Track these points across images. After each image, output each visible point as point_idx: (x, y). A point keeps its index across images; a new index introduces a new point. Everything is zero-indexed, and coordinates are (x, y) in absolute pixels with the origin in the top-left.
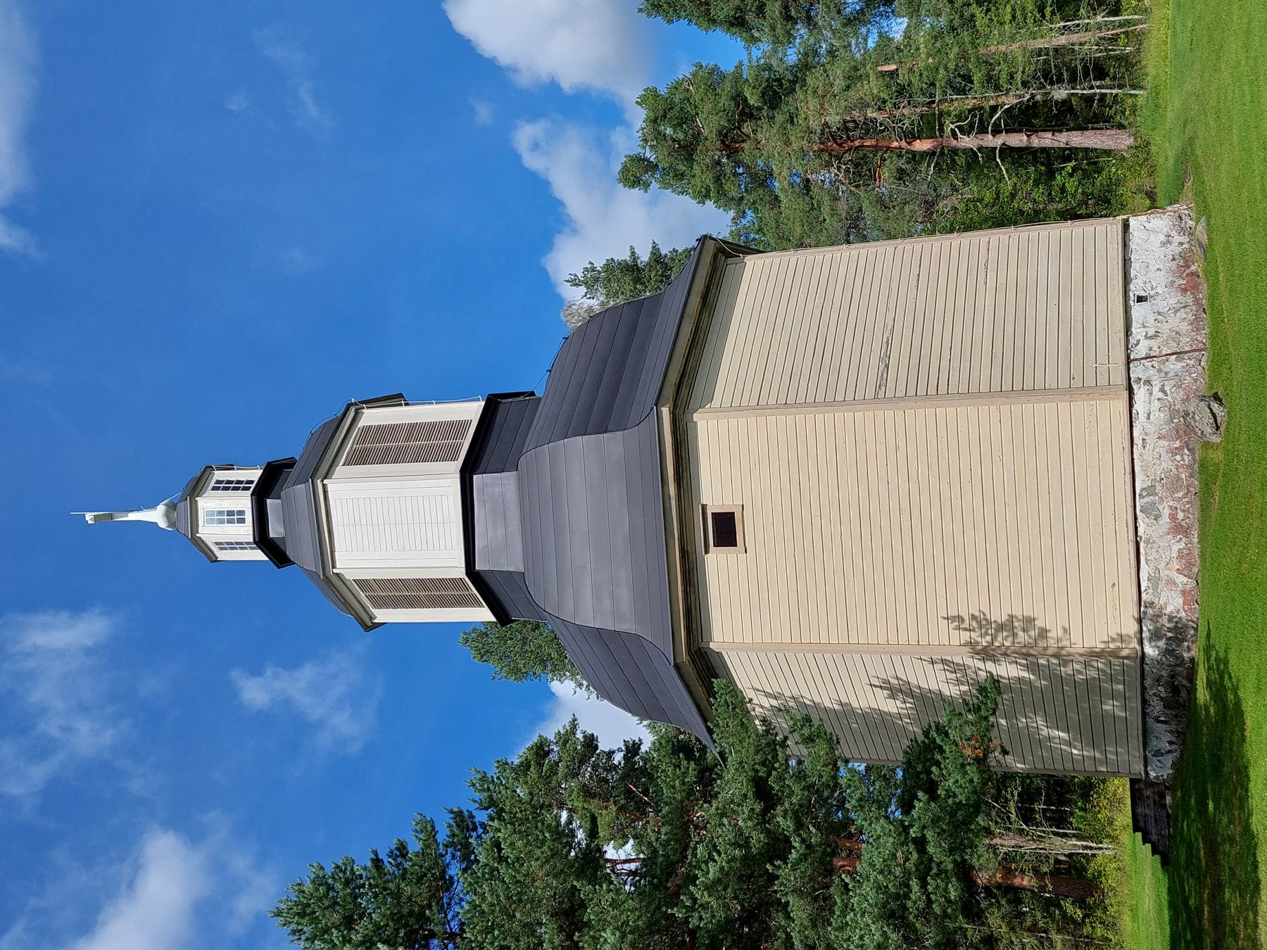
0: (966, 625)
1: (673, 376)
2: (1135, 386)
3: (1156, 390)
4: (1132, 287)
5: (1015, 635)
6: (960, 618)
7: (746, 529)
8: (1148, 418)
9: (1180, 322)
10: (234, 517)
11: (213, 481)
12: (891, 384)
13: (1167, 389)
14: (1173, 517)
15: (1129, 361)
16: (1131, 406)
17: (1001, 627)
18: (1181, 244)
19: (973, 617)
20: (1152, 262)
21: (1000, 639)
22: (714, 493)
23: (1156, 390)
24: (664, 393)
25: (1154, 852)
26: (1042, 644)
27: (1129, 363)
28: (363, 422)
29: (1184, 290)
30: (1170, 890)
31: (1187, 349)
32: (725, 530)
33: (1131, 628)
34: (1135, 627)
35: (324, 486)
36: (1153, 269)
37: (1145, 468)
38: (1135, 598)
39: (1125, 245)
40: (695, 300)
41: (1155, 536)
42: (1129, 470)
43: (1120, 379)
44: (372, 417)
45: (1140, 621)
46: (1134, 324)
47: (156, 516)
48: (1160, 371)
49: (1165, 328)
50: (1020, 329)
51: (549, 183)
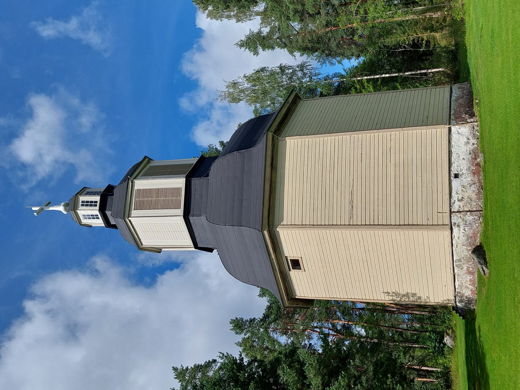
0: (391, 294)
2: (453, 227)
3: (462, 229)
4: (452, 169)
5: (409, 298)
6: (388, 293)
7: (304, 263)
8: (459, 238)
9: (471, 192)
11: (80, 202)
12: (355, 217)
13: (466, 229)
14: (468, 269)
15: (451, 212)
16: (452, 233)
17: (404, 296)
18: (473, 144)
19: (393, 292)
20: (461, 154)
21: (404, 299)
22: (290, 251)
23: (462, 229)
24: (264, 223)
25: (460, 316)
26: (419, 301)
27: (451, 214)
28: (136, 187)
29: (474, 174)
30: (466, 326)
31: (475, 209)
33: (452, 298)
34: (454, 298)
35: (130, 221)
36: (461, 158)
37: (457, 254)
38: (454, 290)
39: (449, 142)
40: (268, 169)
41: (461, 274)
42: (454, 156)
43: (447, 222)
44: (141, 184)
45: (455, 297)
46: (453, 191)
47: (61, 208)
48: (463, 220)
49: (466, 195)
50: (406, 190)
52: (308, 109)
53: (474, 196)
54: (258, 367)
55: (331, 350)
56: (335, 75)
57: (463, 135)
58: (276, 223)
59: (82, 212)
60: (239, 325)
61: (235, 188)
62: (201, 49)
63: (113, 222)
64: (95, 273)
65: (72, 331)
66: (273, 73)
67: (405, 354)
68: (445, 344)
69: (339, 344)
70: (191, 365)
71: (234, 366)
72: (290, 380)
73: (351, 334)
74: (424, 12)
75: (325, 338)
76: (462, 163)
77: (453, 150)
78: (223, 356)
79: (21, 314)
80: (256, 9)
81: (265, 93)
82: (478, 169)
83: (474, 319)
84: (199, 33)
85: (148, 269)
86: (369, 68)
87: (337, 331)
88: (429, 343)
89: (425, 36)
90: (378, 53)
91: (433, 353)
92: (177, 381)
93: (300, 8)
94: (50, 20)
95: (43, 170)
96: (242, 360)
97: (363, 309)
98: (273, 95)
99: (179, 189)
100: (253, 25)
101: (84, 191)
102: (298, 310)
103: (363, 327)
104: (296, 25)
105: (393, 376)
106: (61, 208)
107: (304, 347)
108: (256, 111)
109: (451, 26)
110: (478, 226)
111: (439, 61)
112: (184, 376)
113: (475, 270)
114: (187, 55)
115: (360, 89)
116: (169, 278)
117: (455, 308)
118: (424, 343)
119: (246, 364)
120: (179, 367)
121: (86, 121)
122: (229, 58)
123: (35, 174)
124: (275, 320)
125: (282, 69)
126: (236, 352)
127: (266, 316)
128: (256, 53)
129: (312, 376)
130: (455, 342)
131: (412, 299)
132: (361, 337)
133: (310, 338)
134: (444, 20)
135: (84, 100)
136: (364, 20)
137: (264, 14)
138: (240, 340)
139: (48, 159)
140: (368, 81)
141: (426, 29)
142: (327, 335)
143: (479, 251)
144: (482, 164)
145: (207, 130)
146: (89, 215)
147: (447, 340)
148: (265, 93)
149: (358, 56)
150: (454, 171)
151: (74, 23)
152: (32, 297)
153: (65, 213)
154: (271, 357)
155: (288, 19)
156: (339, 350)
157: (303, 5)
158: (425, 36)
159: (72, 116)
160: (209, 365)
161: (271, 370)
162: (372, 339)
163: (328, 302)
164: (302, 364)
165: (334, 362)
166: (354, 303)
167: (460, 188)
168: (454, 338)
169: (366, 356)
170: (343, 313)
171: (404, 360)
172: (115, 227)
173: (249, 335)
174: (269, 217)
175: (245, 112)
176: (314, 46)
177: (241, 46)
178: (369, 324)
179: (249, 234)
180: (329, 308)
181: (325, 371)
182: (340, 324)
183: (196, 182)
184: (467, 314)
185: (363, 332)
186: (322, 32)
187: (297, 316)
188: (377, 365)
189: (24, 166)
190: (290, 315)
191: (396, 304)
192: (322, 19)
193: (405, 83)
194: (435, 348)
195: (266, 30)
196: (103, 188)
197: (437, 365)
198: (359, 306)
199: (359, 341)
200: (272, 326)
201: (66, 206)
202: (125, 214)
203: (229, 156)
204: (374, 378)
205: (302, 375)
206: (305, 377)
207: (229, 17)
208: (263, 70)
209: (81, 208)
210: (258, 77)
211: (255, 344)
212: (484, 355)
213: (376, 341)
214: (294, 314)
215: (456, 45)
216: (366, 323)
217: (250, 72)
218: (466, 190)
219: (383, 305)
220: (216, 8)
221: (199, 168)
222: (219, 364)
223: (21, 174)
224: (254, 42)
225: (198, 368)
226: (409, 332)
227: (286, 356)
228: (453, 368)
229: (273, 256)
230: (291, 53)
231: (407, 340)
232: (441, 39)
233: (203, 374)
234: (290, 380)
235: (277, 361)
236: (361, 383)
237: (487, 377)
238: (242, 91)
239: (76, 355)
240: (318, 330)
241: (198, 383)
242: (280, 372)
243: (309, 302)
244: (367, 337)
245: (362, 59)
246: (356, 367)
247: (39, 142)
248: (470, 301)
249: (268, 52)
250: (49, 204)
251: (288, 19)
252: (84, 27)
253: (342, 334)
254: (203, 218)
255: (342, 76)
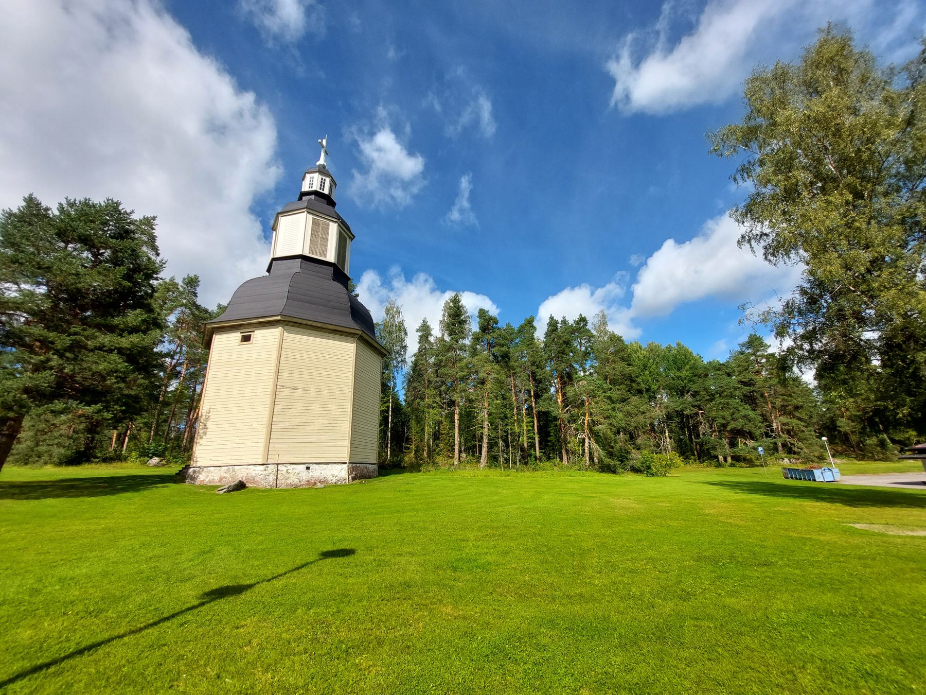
1: (296, 320)
7: (246, 345)
9: (293, 480)
10: (311, 185)
22: (260, 335)
28: (331, 224)
30: (169, 476)
32: (246, 339)
40: (319, 325)
42: (325, 466)
47: (322, 161)
49: (291, 476)
51: (477, 294)
52: (375, 363)
53: (289, 481)
54: (146, 293)
55: (156, 359)
56: (395, 384)
57: (341, 472)
58: (286, 327)
59: (317, 177)
60: (192, 282)
61: (321, 299)
62: (433, 291)
63: (304, 198)
64: (268, 165)
65: (217, 129)
66: (402, 340)
67: (146, 424)
68: (151, 458)
69: (162, 367)
70: (156, 233)
71: (150, 271)
72: (129, 319)
73: (170, 378)
74: (428, 446)
75: (170, 355)
76: (318, 472)
77: (329, 466)
78: (163, 263)
79: (242, 86)
80: (446, 335)
81: (390, 333)
82: (311, 485)
83: (175, 482)
84: (443, 292)
85: (265, 214)
86: (397, 408)
87: (175, 366)
88: (154, 444)
89: (413, 447)
90: (405, 415)
91: (143, 448)
92: (142, 218)
93: (443, 364)
94: (471, 187)
95: (367, 148)
96: (157, 279)
97: (195, 390)
98: (388, 339)
99: (325, 255)
100: (437, 331)
101: (333, 183)
102: (201, 336)
103: (177, 389)
104: (432, 360)
105: (122, 411)
106: (322, 161)
107: (162, 336)
108: (378, 324)
109: (417, 463)
110: (263, 484)
111: (395, 456)
112: (144, 224)
113: (223, 483)
114: (431, 280)
115: (384, 401)
116: (257, 228)
117: (188, 467)
118: (154, 440)
119: (151, 282)
120: (155, 222)
121: (398, 193)
122: (417, 310)
123: (364, 141)
124: (193, 314)
125: (405, 347)
126: (165, 275)
127: (198, 307)
128: (418, 331)
129: (132, 339)
130: (154, 466)
131: (201, 431)
132: (167, 386)
133: (171, 342)
134: (421, 459)
135: (415, 197)
136: (429, 406)
137: (442, 340)
138: (176, 281)
139: (375, 155)
140: (388, 407)
141: (417, 447)
142: (172, 358)
143: (241, 486)
144: (315, 487)
145: (373, 282)
146: (313, 182)
147: (156, 460)
148: (390, 333)
149: (405, 401)
150: (311, 466)
151: (466, 204)
152: (258, 102)
153: (318, 163)
154: (155, 305)
155: (437, 356)
156: (155, 366)
157: (444, 366)
158: (413, 447)
159: (405, 185)
160: (155, 249)
161: (142, 303)
162: (163, 396)
163: (206, 361)
164: (145, 332)
165: (143, 361)
166: (202, 383)
167: (297, 471)
168: (157, 466)
169: (146, 388)
170: (193, 373)
171: (140, 421)
172: (300, 199)
173: (181, 289)
174: (290, 322)
175: (377, 315)
176: (417, 371)
177: (424, 321)
178: (179, 397)
179: (278, 305)
180: (199, 364)
181: (135, 352)
182: (183, 370)
183: (330, 270)
184: (181, 477)
185: (171, 389)
186: (425, 377)
187: (195, 333)
188: (136, 398)
189: (372, 134)
190: (196, 327)
191: (197, 418)
192: (434, 378)
193: (383, 433)
194: (149, 449)
195: (432, 339)
196: (333, 197)
197: (130, 450)
198: (198, 388)
199: (162, 385)
200: (188, 311)
201: (324, 167)
202: (310, 209)
203: (347, 297)
204: (122, 395)
205: (133, 330)
206: (130, 333)
207: (444, 315)
208: (406, 334)
209: (320, 177)
210: (401, 329)
211: (171, 293)
212: (138, 491)
213: (161, 399)
214: (197, 331)
215: (404, 467)
216: (181, 392)
217: (406, 325)
218: (296, 475)
219: (197, 407)
220: (450, 308)
221: (339, 274)
222: (153, 258)
223: (366, 130)
224: (425, 331)
225: (153, 239)
226: (166, 428)
227: (155, 319)
228: (124, 464)
229: (256, 321)
230: (415, 355)
231: (158, 425)
232: (409, 458)
233: (146, 242)
234: (129, 319)
235: (150, 310)
236: (118, 382)
237: (113, 494)
238: (393, 317)
239: (191, 126)
240: (178, 350)
241: (136, 236)
242: (138, 311)
243: (208, 345)
244: (166, 391)
245: (403, 403)
246: (135, 380)
247: (387, 151)
248: (193, 479)
249: (417, 340)
250: (326, 153)
251: (437, 356)
252: (462, 211)
253: (171, 370)
254: (299, 270)
255: (393, 389)
